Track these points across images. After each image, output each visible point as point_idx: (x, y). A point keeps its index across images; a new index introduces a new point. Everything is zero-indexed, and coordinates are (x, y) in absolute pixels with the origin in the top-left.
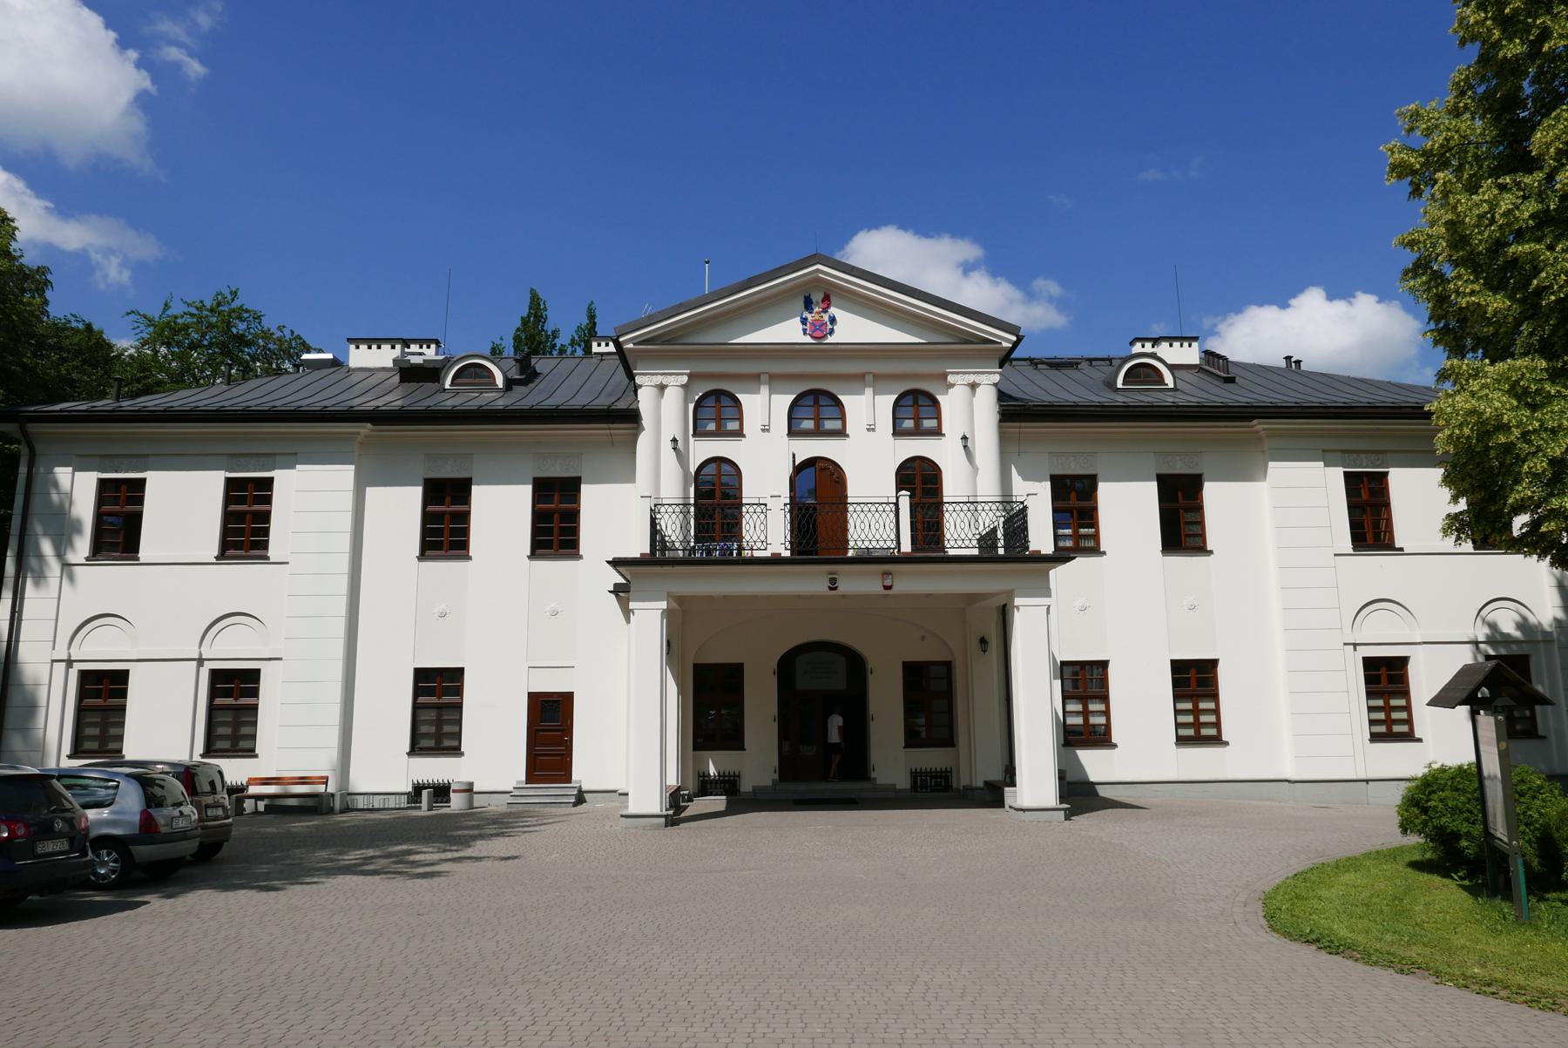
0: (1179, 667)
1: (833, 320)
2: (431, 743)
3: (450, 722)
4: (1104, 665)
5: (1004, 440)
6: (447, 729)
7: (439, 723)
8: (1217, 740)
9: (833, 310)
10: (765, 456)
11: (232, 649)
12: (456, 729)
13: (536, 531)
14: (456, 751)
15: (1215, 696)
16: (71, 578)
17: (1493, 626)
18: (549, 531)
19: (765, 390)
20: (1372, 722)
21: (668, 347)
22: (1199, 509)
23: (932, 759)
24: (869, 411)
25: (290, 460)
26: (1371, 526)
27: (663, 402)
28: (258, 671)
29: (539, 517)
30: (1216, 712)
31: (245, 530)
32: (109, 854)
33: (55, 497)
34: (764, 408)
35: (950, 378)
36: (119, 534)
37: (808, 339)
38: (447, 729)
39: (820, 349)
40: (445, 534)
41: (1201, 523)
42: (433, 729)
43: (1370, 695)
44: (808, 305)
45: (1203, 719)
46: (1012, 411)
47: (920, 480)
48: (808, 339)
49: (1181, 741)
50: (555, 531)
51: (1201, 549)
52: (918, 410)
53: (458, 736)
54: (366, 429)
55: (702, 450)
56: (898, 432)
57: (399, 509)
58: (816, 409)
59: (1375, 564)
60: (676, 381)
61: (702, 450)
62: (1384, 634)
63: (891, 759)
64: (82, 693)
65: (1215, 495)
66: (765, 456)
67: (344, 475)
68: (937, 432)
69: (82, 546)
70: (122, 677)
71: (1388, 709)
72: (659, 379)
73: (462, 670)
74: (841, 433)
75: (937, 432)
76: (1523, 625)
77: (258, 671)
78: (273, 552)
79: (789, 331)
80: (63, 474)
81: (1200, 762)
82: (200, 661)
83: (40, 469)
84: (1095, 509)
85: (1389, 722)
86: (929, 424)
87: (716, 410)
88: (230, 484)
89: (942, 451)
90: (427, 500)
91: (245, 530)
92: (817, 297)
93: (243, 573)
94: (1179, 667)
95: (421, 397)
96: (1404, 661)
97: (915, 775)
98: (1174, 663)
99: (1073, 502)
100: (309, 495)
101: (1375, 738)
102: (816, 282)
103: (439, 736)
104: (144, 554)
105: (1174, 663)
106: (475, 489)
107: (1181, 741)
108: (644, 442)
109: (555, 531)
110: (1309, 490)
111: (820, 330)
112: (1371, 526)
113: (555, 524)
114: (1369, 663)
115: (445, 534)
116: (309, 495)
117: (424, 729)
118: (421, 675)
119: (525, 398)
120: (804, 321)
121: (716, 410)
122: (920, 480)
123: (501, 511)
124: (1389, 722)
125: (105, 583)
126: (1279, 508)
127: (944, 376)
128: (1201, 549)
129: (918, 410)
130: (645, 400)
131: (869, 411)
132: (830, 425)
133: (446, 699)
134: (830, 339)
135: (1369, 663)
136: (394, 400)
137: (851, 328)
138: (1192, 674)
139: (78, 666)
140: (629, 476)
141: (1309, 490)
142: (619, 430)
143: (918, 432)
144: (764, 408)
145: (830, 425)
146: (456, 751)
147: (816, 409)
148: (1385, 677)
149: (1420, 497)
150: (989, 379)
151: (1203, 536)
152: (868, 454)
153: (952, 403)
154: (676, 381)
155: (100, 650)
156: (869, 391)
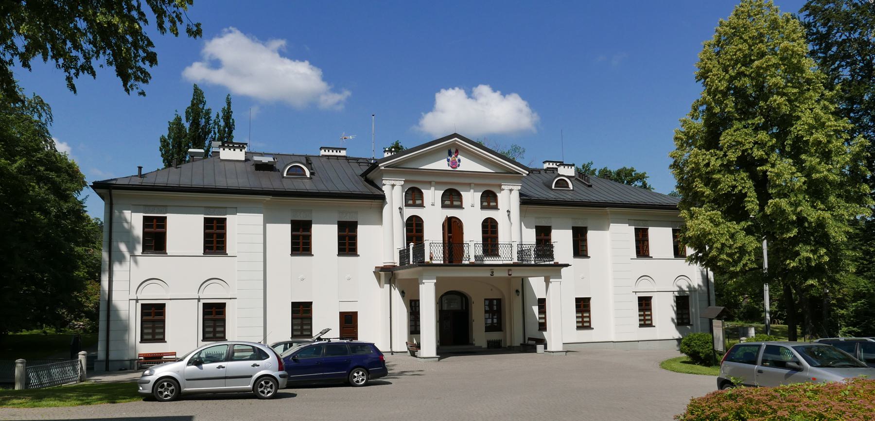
0: (578, 300)
1: (459, 161)
2: (150, 337)
3: (306, 324)
4: (589, 299)
5: (521, 211)
6: (218, 329)
7: (215, 327)
8: (589, 327)
9: (459, 156)
10: (433, 215)
11: (213, 294)
12: (222, 329)
13: (206, 242)
14: (163, 340)
15: (589, 311)
16: (136, 262)
17: (680, 287)
18: (212, 242)
19: (433, 188)
20: (577, 322)
21: (396, 170)
22: (586, 240)
23: (495, 336)
24: (471, 198)
25: (235, 211)
26: (642, 249)
27: (393, 191)
28: (225, 304)
29: (294, 238)
30: (589, 317)
31: (215, 241)
32: (358, 373)
33: (126, 225)
34: (432, 196)
35: (503, 187)
36: (155, 241)
37: (450, 169)
38: (218, 329)
39: (453, 174)
40: (301, 244)
41: (586, 246)
42: (212, 329)
43: (577, 312)
44: (450, 154)
45: (585, 319)
46: (526, 201)
47: (490, 228)
48: (450, 169)
49: (578, 328)
50: (347, 245)
51: (585, 256)
52: (489, 199)
53: (164, 333)
54: (268, 198)
55: (409, 212)
56: (483, 208)
57: (281, 234)
58: (452, 198)
59: (643, 262)
60: (399, 183)
61: (409, 212)
62: (645, 288)
63: (480, 336)
64: (143, 314)
65: (591, 235)
66: (433, 215)
67: (259, 218)
68: (496, 208)
69: (139, 249)
70: (223, 306)
71: (583, 317)
72: (393, 182)
73: (311, 303)
74: (422, 206)
75: (496, 208)
76: (689, 287)
77: (225, 304)
78: (229, 250)
79: (442, 165)
80: (127, 214)
81: (585, 336)
82: (199, 300)
83: (116, 213)
84: (356, 236)
85: (583, 322)
86: (418, 202)
87: (414, 196)
88: (206, 220)
89: (498, 215)
90: (340, 230)
91: (215, 241)
92: (453, 150)
93: (215, 261)
94: (578, 300)
95: (266, 182)
96: (650, 298)
97: (489, 342)
98: (576, 299)
99: (543, 236)
100: (242, 226)
101: (641, 326)
102: (454, 144)
103: (215, 332)
104: (169, 250)
105: (576, 299)
106: (313, 226)
107: (578, 328)
108: (386, 210)
109: (347, 245)
110: (621, 234)
111: (454, 164)
112: (642, 249)
113: (347, 241)
114: (640, 299)
115: (301, 244)
116: (242, 226)
117: (146, 331)
118: (294, 305)
119: (174, 177)
120: (448, 160)
121: (414, 196)
122: (490, 228)
123: (325, 235)
124: (583, 322)
125: (151, 264)
126: (612, 240)
127: (500, 186)
128: (585, 256)
129: (489, 199)
130: (386, 189)
131: (471, 198)
132: (455, 203)
133: (305, 315)
134: (458, 169)
135: (640, 299)
136: (242, 183)
137: (467, 165)
138: (582, 303)
139: (140, 302)
140: (379, 221)
141: (621, 234)
142: (376, 203)
143: (452, 206)
144: (432, 196)
145: (455, 203)
146: (163, 340)
147: (452, 198)
148: (645, 304)
149: (661, 238)
150: (517, 188)
151: (586, 251)
152: (471, 215)
153: (502, 197)
154: (399, 183)
155: (152, 294)
156: (472, 191)
